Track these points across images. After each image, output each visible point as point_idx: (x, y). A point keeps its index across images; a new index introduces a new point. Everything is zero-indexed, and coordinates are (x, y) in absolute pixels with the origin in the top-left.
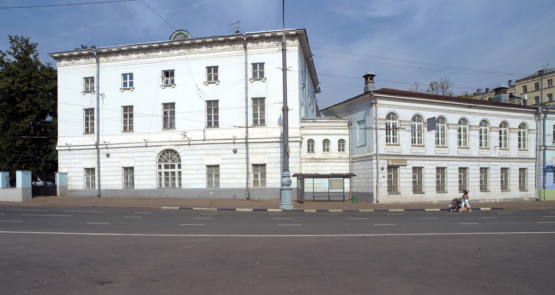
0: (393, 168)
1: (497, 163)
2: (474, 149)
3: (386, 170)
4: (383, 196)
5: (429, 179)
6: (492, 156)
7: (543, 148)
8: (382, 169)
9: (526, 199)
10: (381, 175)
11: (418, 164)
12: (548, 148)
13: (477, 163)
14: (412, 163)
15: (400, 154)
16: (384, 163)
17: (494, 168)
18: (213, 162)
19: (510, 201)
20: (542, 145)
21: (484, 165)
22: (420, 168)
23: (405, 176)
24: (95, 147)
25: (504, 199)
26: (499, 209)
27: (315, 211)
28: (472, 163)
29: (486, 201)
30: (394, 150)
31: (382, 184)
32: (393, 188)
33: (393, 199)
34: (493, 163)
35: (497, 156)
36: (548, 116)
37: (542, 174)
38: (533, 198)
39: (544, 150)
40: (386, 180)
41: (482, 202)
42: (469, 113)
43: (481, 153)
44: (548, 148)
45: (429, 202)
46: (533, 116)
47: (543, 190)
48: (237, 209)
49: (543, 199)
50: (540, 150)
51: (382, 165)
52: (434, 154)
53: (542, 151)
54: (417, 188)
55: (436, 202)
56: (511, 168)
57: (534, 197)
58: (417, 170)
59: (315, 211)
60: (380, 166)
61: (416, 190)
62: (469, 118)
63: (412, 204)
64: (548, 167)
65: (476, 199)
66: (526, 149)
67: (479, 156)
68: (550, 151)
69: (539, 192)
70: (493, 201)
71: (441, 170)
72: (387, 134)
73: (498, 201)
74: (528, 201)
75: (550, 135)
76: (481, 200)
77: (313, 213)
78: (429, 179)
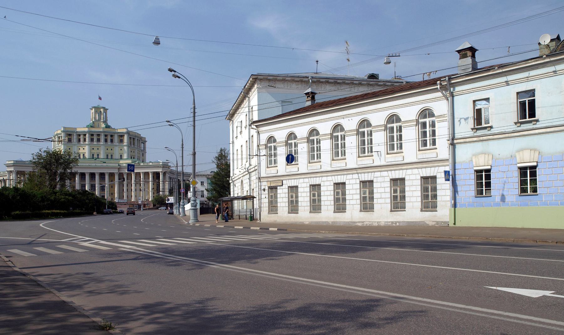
0: (273, 189)
1: (385, 174)
2: (352, 158)
3: (266, 192)
5: (382, 193)
6: (375, 164)
8: (264, 190)
9: (431, 224)
10: (263, 196)
11: (293, 183)
13: (356, 176)
14: (288, 183)
15: (277, 175)
16: (265, 185)
17: (380, 179)
18: (527, 160)
19: (401, 224)
21: (366, 177)
22: (403, 180)
23: (282, 194)
24: (247, 173)
25: (392, 222)
26: (283, 230)
27: (259, 228)
28: (350, 177)
29: (365, 223)
30: (272, 171)
32: (273, 207)
34: (378, 174)
35: (383, 163)
36: (458, 89)
40: (267, 200)
41: (360, 224)
42: (343, 117)
43: (359, 163)
45: (317, 222)
46: (439, 94)
48: (270, 229)
52: (307, 171)
54: (293, 207)
55: (307, 223)
58: (294, 189)
61: (366, 208)
62: (318, 126)
63: (285, 224)
65: (354, 220)
67: (357, 167)
68: (463, 145)
70: (376, 224)
71: (315, 188)
72: (344, 143)
73: (382, 224)
74: (432, 226)
75: (466, 119)
76: (359, 222)
77: (275, 231)
78: (382, 193)
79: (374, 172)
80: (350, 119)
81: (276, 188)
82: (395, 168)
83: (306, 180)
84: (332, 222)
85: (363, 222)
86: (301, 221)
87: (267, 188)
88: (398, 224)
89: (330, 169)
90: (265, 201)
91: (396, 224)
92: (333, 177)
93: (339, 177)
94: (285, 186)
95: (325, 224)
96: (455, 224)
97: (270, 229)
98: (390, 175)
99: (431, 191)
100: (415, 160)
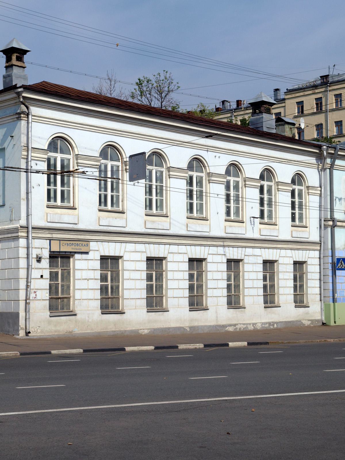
0: (60, 258)
3: (45, 263)
4: (39, 321)
7: (331, 223)
8: (39, 259)
9: (307, 323)
10: (36, 274)
11: (111, 249)
12: (339, 224)
14: (101, 248)
17: (252, 259)
20: (329, 217)
23: (85, 273)
25: (269, 323)
26: (261, 344)
27: (245, 344)
29: (238, 327)
31: (39, 293)
32: (60, 302)
33: (62, 326)
35: (257, 236)
37: (330, 273)
38: (318, 321)
39: (334, 226)
40: (45, 283)
41: (231, 329)
42: (208, 148)
43: (229, 230)
44: (339, 224)
45: (132, 331)
47: (332, 304)
48: (231, 344)
49: (332, 324)
50: (326, 227)
51: (38, 252)
52: (143, 230)
53: (329, 229)
55: (146, 332)
56: (308, 263)
57: (318, 317)
58: (110, 263)
59: (201, 346)
60: (34, 253)
63: (98, 337)
64: (338, 260)
66: (304, 224)
69: (326, 309)
71: (155, 263)
73: (259, 327)
74: (309, 327)
76: (230, 325)
79: (245, 247)
80: (218, 155)
81: (66, 256)
82: (209, 243)
83: (141, 247)
84: (191, 328)
85: (235, 325)
86: (129, 328)
87: (46, 254)
88: (275, 326)
89: (184, 232)
90: (41, 287)
91: (273, 325)
92: (188, 247)
93: (112, 245)
94: (95, 256)
95: (178, 333)
96: (335, 322)
97: (181, 347)
98: (101, 249)
99: (299, 283)
100: (289, 238)
